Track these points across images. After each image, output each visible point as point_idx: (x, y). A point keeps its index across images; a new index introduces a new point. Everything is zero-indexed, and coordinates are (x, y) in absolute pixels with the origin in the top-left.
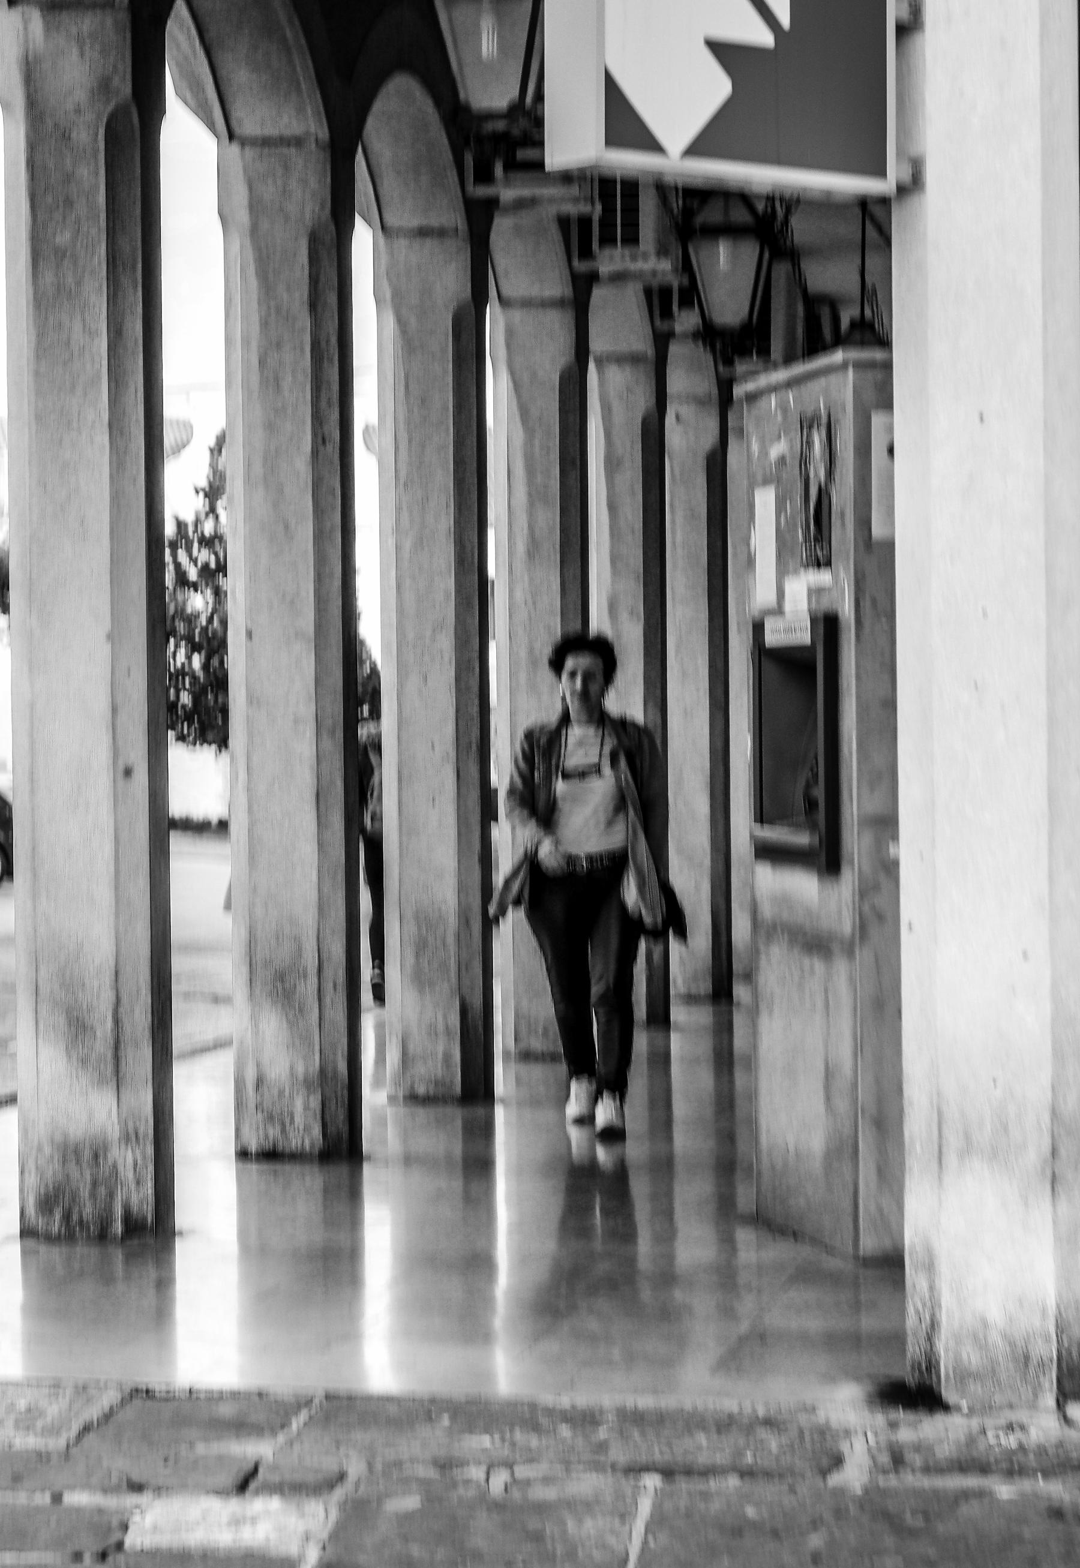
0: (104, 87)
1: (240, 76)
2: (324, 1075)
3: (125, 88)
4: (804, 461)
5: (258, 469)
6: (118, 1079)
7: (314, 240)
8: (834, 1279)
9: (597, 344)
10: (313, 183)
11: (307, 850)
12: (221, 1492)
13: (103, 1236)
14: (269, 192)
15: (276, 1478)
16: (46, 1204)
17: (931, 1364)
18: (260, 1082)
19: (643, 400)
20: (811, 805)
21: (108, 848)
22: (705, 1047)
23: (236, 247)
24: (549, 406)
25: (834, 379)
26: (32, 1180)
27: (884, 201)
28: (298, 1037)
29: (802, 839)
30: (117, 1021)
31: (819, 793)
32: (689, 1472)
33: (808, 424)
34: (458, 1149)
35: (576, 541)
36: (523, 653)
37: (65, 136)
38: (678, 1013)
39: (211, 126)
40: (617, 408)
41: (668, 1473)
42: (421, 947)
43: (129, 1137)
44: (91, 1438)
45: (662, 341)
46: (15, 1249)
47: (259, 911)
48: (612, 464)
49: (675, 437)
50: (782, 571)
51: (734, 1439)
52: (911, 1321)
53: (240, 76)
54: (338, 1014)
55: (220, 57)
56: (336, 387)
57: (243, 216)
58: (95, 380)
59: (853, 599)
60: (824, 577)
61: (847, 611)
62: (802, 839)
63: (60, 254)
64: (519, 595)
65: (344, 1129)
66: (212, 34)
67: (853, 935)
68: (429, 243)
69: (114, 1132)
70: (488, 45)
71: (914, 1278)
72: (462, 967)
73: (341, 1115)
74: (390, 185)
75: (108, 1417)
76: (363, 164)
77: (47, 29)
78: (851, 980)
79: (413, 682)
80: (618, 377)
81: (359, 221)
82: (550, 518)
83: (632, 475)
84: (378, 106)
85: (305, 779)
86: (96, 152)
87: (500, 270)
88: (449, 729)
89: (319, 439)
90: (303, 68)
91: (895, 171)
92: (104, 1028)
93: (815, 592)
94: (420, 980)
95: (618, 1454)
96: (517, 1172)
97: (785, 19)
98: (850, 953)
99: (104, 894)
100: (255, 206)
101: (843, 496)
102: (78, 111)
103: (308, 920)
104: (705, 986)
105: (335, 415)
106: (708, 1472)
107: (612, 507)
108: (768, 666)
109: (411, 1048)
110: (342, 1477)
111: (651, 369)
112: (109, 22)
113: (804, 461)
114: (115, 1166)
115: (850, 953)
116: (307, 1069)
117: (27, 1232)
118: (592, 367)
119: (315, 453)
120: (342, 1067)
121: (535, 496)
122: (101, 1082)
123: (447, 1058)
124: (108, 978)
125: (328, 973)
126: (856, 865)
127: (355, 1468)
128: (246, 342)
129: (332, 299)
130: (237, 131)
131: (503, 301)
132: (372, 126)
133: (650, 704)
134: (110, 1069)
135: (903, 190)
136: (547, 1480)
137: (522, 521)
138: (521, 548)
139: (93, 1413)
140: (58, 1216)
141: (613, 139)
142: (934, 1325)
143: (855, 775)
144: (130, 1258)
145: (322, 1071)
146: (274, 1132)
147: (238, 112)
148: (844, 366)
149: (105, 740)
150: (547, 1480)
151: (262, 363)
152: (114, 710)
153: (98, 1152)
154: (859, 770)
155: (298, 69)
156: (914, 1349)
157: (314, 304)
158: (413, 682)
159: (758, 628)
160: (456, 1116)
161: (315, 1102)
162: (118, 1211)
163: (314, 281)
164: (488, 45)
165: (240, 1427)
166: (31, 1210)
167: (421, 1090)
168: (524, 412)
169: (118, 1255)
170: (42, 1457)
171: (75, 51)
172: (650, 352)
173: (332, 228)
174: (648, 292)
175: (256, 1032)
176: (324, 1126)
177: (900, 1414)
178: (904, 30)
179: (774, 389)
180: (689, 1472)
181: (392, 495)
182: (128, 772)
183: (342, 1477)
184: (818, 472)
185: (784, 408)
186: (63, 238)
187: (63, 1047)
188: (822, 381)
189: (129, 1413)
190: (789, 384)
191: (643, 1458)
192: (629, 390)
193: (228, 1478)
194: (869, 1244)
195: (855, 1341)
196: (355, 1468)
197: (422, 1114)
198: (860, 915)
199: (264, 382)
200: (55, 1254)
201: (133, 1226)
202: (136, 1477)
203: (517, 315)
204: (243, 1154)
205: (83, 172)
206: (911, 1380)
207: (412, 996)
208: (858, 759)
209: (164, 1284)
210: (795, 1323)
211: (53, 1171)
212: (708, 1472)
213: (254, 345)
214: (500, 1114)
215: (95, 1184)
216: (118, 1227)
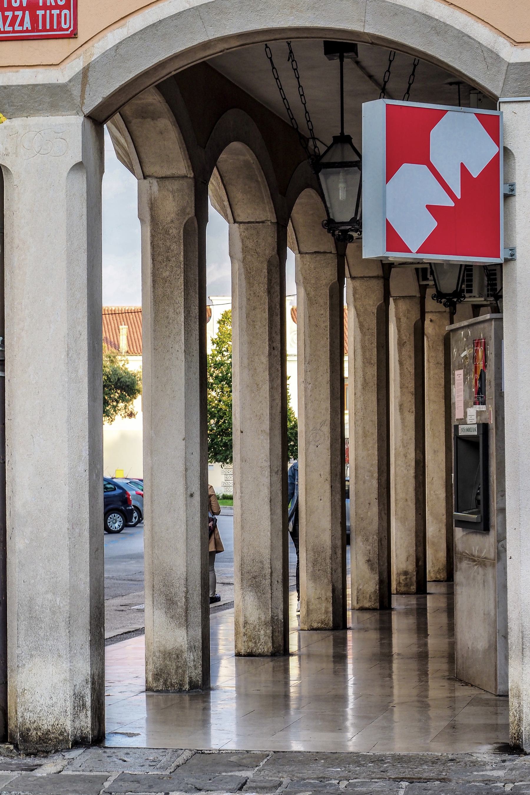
0: (183, 211)
1: (238, 195)
2: (273, 620)
3: (191, 211)
4: (475, 358)
5: (246, 361)
6: (187, 624)
7: (270, 263)
8: (486, 703)
9: (394, 292)
10: (270, 240)
11: (266, 524)
12: (231, 791)
13: (180, 691)
14: (250, 244)
15: (254, 785)
16: (157, 676)
17: (519, 736)
18: (246, 623)
19: (415, 316)
20: (478, 502)
21: (184, 527)
22: (443, 603)
23: (237, 266)
24: (372, 323)
25: (486, 325)
26: (151, 667)
27: (501, 265)
28: (262, 604)
29: (474, 517)
30: (186, 598)
31: (481, 497)
32: (420, 780)
33: (477, 343)
34: (331, 651)
35: (384, 383)
36: (360, 432)
37: (167, 232)
38: (431, 588)
39: (226, 217)
40: (404, 320)
41: (411, 780)
42: (315, 563)
43: (191, 648)
44: (179, 770)
45: (423, 289)
46: (144, 696)
47: (245, 550)
48: (401, 344)
49: (429, 328)
50: (466, 405)
51: (438, 767)
52: (511, 719)
53: (238, 195)
54: (279, 594)
55: (230, 188)
56: (279, 327)
57: (239, 255)
58: (178, 334)
59: (494, 418)
60: (483, 408)
61: (492, 422)
62: (474, 517)
63: (165, 280)
64: (359, 406)
65: (282, 644)
66: (226, 179)
67: (495, 557)
68: (319, 257)
69: (185, 647)
70: (342, 195)
71: (513, 701)
72: (333, 571)
73: (280, 638)
74: (302, 230)
75: (187, 761)
76: (291, 224)
77: (159, 190)
78: (494, 577)
79: (312, 448)
80: (403, 306)
81: (289, 250)
82: (373, 371)
83: (410, 348)
84: (298, 201)
85: (265, 492)
86: (179, 239)
87: (351, 264)
88: (328, 468)
89: (272, 348)
90: (266, 193)
91: (503, 254)
92: (182, 603)
93: (479, 413)
94: (314, 577)
95: (392, 774)
96: (356, 660)
97: (459, 197)
98: (493, 566)
99: (181, 546)
100: (245, 250)
101: (490, 375)
102: (172, 221)
103: (266, 553)
104: (443, 576)
105: (278, 338)
106: (428, 780)
107: (401, 363)
108: (462, 445)
109: (311, 607)
110: (280, 784)
111: (418, 301)
112: (185, 184)
113: (475, 358)
114: (185, 661)
115: (493, 566)
116: (266, 618)
117: (148, 689)
118: (391, 300)
119: (270, 354)
120: (281, 617)
121: (366, 361)
122: (180, 625)
123: (326, 612)
124: (183, 582)
125: (274, 575)
126: (496, 529)
127: (286, 781)
128: (240, 308)
129: (278, 288)
130: (238, 219)
131: (353, 278)
132: (296, 209)
133: (418, 452)
134: (183, 621)
135: (507, 260)
136: (363, 784)
137: (360, 373)
138: (359, 386)
139: (180, 761)
140: (162, 680)
141: (389, 249)
142: (520, 720)
143: (495, 489)
144: (192, 698)
145: (272, 618)
146: (251, 644)
147: (238, 211)
148: (490, 320)
149: (182, 482)
150: (363, 784)
151: (248, 316)
152: (186, 470)
153: (178, 655)
154: (497, 489)
155: (263, 192)
156: (512, 730)
157: (269, 292)
158: (312, 448)
159: (456, 427)
160: (330, 636)
161: (269, 632)
162: (187, 680)
163: (270, 281)
164: (342, 195)
165: (240, 766)
166: (150, 679)
167: (315, 625)
168: (361, 326)
169: (187, 697)
170: (160, 778)
171: (171, 198)
172: (418, 295)
173: (277, 256)
174: (417, 270)
175: (244, 600)
176: (273, 643)
177: (506, 757)
178: (507, 197)
179: (462, 328)
180: (420, 780)
181: (303, 367)
182: (192, 495)
183: (280, 784)
184: (481, 365)
185: (466, 335)
186: (166, 274)
187: (163, 611)
188: (482, 326)
189: (193, 761)
190: (468, 326)
191: (401, 776)
192: (408, 311)
193: (234, 786)
194: (501, 688)
195: (495, 728)
196: (286, 781)
197: (316, 635)
198: (497, 549)
199: (248, 323)
200: (161, 697)
201: (193, 686)
202: (197, 786)
203: (358, 283)
204: (238, 655)
205: (174, 247)
206: (511, 742)
207: (311, 585)
208: (497, 483)
209: (206, 709)
210: (473, 721)
211: (159, 663)
212: (428, 780)
213: (244, 310)
214: (350, 634)
215: (178, 667)
216: (187, 687)
